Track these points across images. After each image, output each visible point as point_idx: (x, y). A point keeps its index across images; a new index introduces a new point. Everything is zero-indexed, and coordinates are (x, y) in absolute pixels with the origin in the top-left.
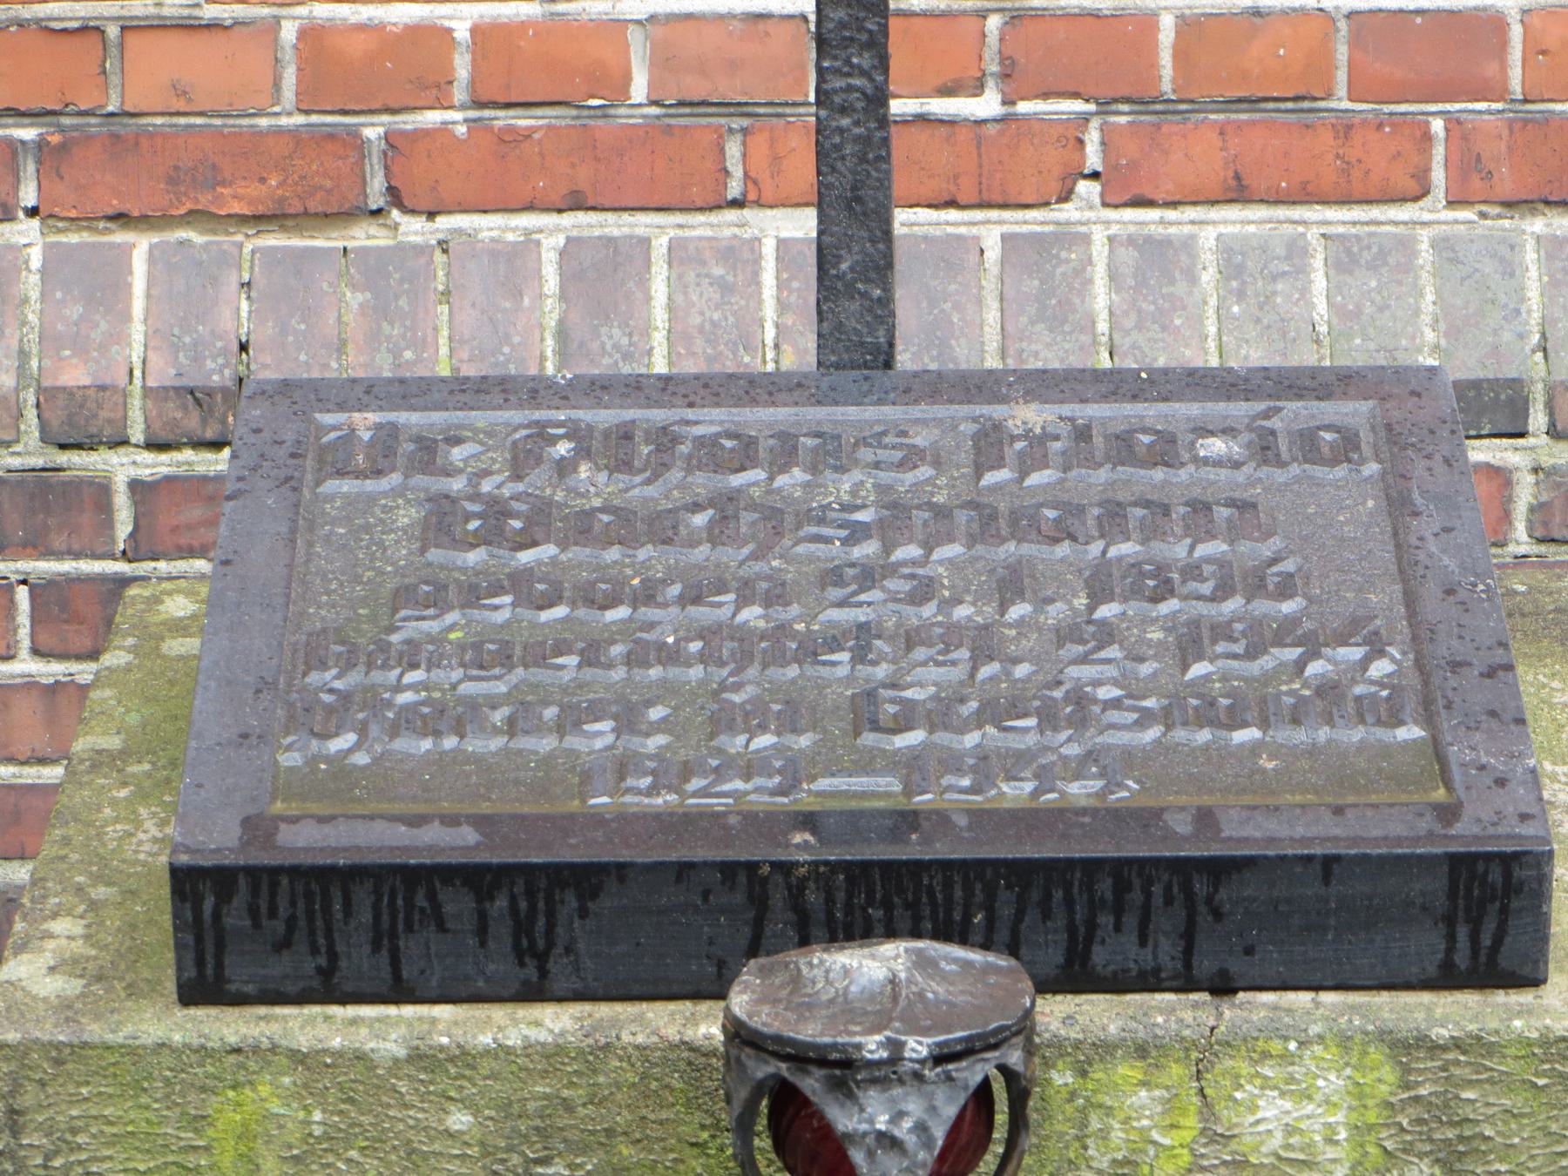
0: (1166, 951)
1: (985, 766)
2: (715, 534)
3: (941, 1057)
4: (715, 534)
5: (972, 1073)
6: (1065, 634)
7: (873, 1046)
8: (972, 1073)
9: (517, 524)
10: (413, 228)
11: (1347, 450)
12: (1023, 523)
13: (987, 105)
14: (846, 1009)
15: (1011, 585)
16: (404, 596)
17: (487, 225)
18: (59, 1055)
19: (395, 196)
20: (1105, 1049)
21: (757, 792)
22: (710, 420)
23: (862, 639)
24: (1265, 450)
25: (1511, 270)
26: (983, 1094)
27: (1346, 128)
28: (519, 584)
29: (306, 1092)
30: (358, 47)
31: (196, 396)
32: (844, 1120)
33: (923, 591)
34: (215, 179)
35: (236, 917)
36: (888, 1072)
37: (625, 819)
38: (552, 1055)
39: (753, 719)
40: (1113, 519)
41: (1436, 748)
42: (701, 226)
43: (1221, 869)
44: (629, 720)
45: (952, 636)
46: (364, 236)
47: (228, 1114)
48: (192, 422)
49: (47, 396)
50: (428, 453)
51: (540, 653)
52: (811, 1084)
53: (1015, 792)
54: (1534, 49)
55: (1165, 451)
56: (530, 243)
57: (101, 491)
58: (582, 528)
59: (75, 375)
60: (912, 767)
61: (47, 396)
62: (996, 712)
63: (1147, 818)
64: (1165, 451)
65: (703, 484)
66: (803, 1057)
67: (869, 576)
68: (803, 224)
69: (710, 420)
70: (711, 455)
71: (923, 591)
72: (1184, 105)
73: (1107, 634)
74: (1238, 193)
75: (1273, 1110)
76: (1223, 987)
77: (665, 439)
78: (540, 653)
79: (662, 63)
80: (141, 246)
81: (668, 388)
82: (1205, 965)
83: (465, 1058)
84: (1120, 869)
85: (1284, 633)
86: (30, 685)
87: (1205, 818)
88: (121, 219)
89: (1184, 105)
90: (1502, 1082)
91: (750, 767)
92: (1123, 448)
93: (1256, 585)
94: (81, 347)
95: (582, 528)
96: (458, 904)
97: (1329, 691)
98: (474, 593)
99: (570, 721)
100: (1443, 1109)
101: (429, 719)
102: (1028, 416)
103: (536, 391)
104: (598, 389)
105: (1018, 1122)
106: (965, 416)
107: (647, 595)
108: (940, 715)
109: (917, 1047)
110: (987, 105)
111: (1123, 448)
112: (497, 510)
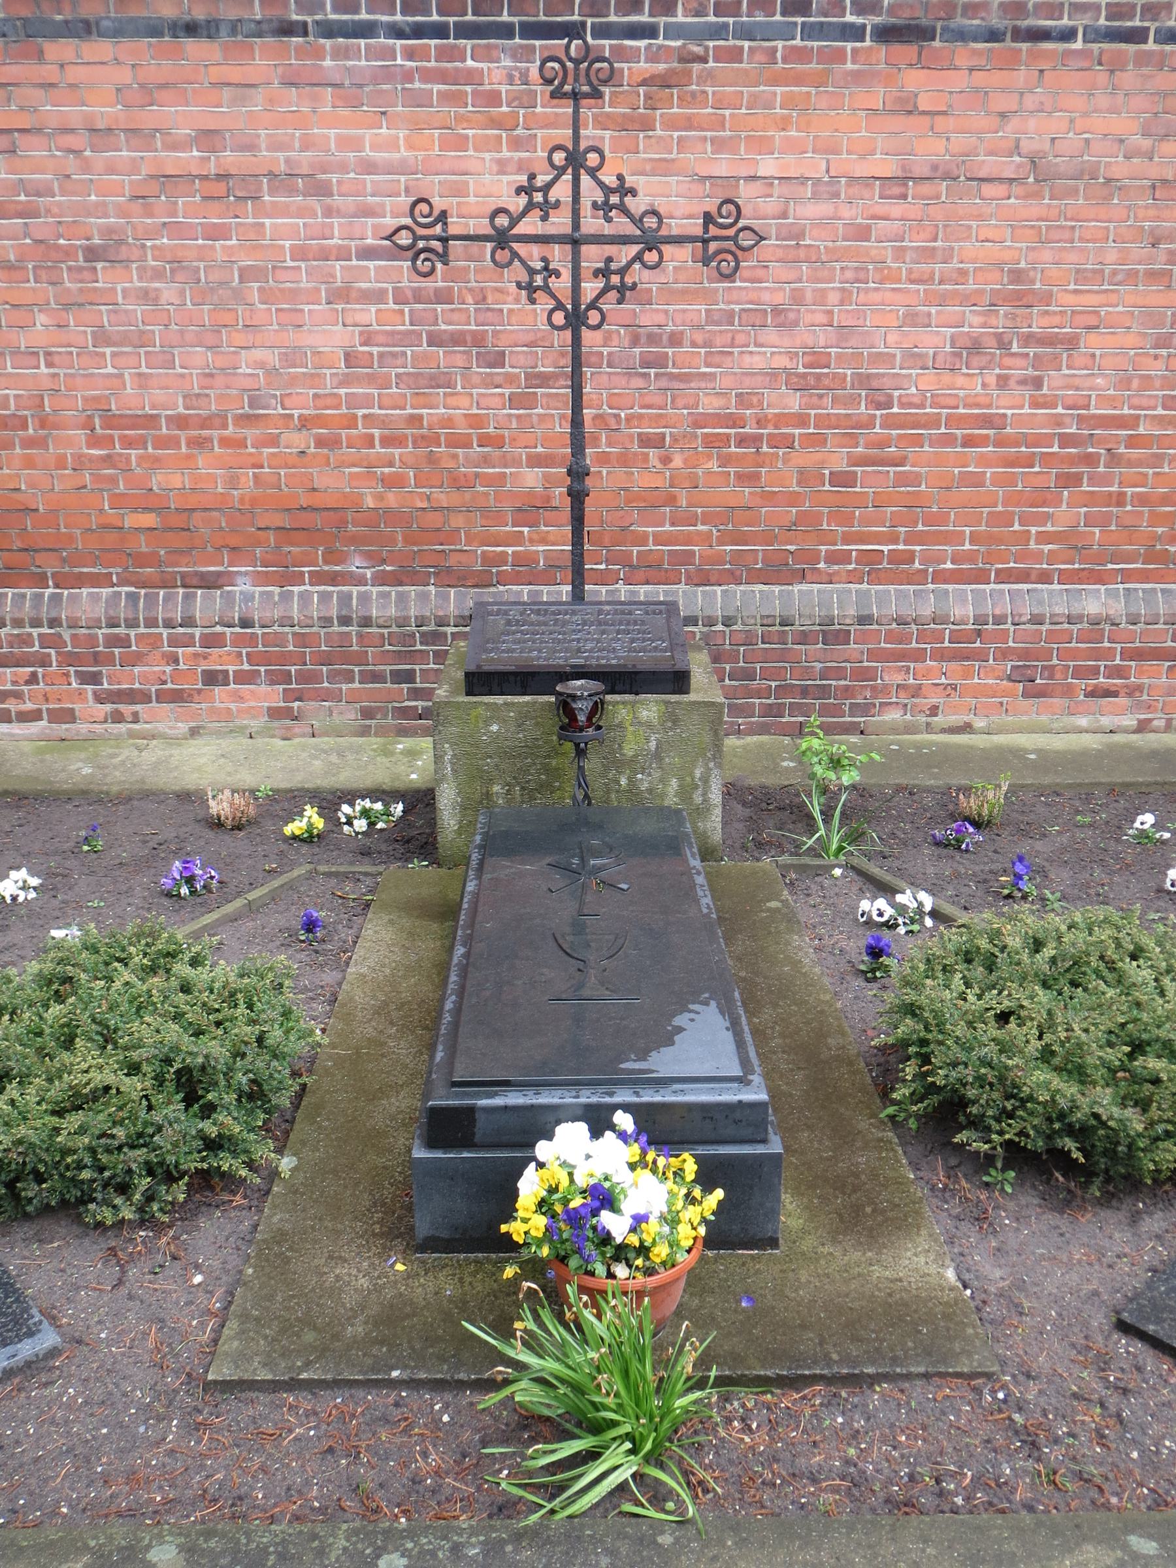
0: (628, 687)
1: (598, 658)
2: (554, 625)
3: (590, 695)
4: (554, 625)
5: (596, 698)
6: (612, 639)
7: (579, 693)
8: (596, 698)
9: (437, 1407)
10: (501, 588)
11: (661, 612)
12: (606, 624)
13: (603, 567)
14: (574, 688)
15: (603, 632)
16: (503, 633)
17: (514, 588)
18: (447, 703)
19: (498, 583)
20: (618, 703)
21: (561, 662)
22: (553, 608)
23: (578, 640)
24: (647, 613)
25: (696, 596)
26: (596, 702)
27: (666, 571)
28: (522, 632)
29: (486, 710)
30: (491, 555)
31: (462, 617)
32: (574, 706)
33: (589, 633)
34: (465, 578)
35: (475, 681)
36: (581, 698)
37: (539, 666)
38: (528, 703)
39: (560, 651)
40: (620, 624)
41: (673, 657)
42: (552, 588)
43: (636, 673)
44: (540, 651)
45: (594, 639)
46: (492, 589)
47: (474, 713)
48: (462, 622)
49: (436, 617)
50: (506, 613)
51: (524, 642)
52: (569, 700)
53: (604, 662)
54: (700, 556)
55: (630, 613)
56: (522, 591)
57: (445, 634)
58: (532, 624)
59: (441, 613)
60: (586, 658)
61: (436, 617)
62: (600, 650)
63: (625, 665)
64: (630, 613)
65: (552, 617)
66: (569, 695)
67: (579, 631)
68: (569, 588)
69: (553, 608)
70: (554, 613)
71: (589, 633)
72: (638, 567)
73: (619, 639)
74: (647, 583)
75: (645, 713)
76: (637, 694)
77: (546, 611)
78: (524, 642)
79: (545, 559)
80: (452, 591)
81: (546, 603)
82: (634, 690)
83: (513, 704)
84: (620, 673)
85: (649, 639)
86: (432, 669)
87: (634, 666)
88: (449, 586)
89: (638, 567)
90: (683, 709)
91: (560, 658)
92: (623, 613)
93: (644, 632)
94: (442, 608)
95: (532, 624)
96: (512, 678)
97: (656, 648)
98: (514, 633)
99: (531, 651)
100: (673, 714)
101: (508, 651)
102: (608, 608)
103: (524, 604)
104: (535, 603)
105: (602, 708)
106: (597, 607)
107: (543, 633)
108: (590, 651)
109: (586, 694)
110: (603, 567)
111: (623, 613)
112: (518, 621)
